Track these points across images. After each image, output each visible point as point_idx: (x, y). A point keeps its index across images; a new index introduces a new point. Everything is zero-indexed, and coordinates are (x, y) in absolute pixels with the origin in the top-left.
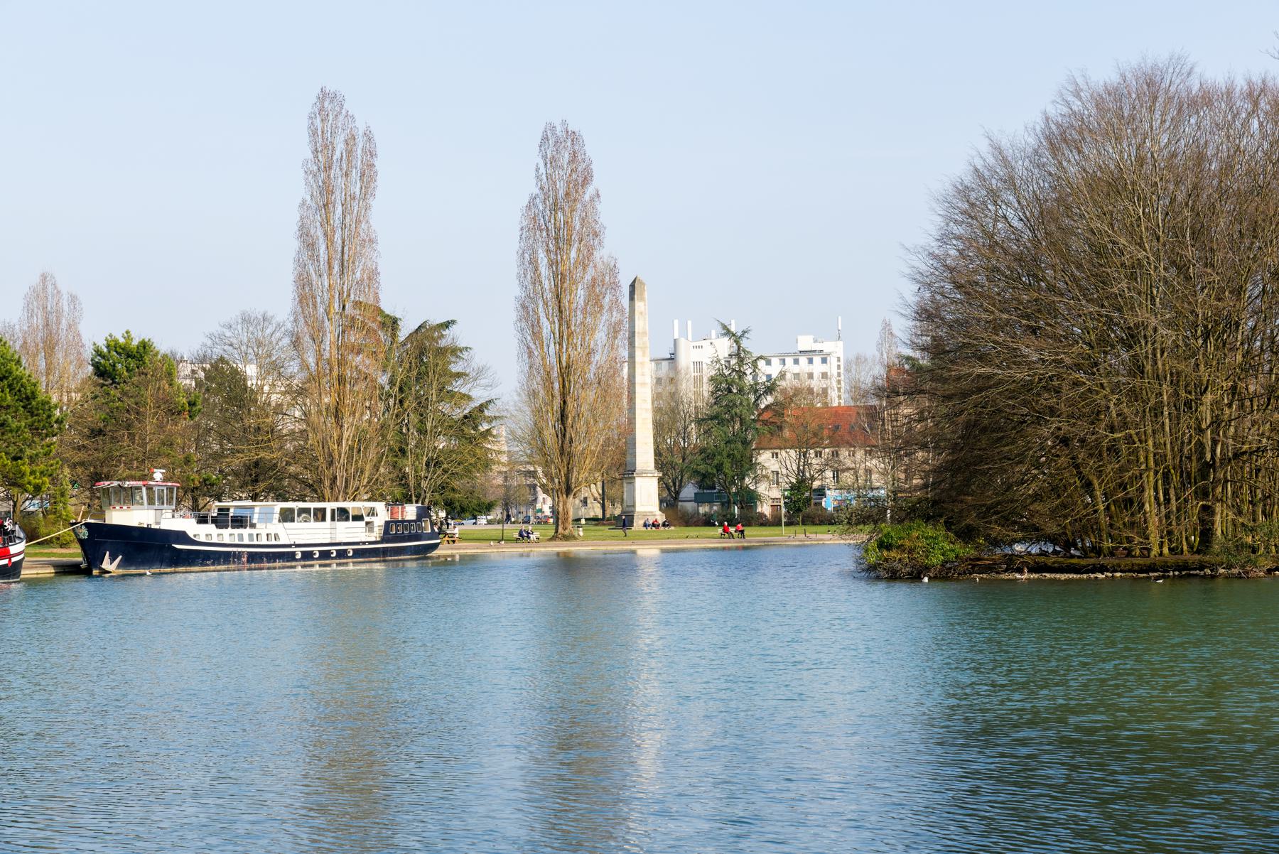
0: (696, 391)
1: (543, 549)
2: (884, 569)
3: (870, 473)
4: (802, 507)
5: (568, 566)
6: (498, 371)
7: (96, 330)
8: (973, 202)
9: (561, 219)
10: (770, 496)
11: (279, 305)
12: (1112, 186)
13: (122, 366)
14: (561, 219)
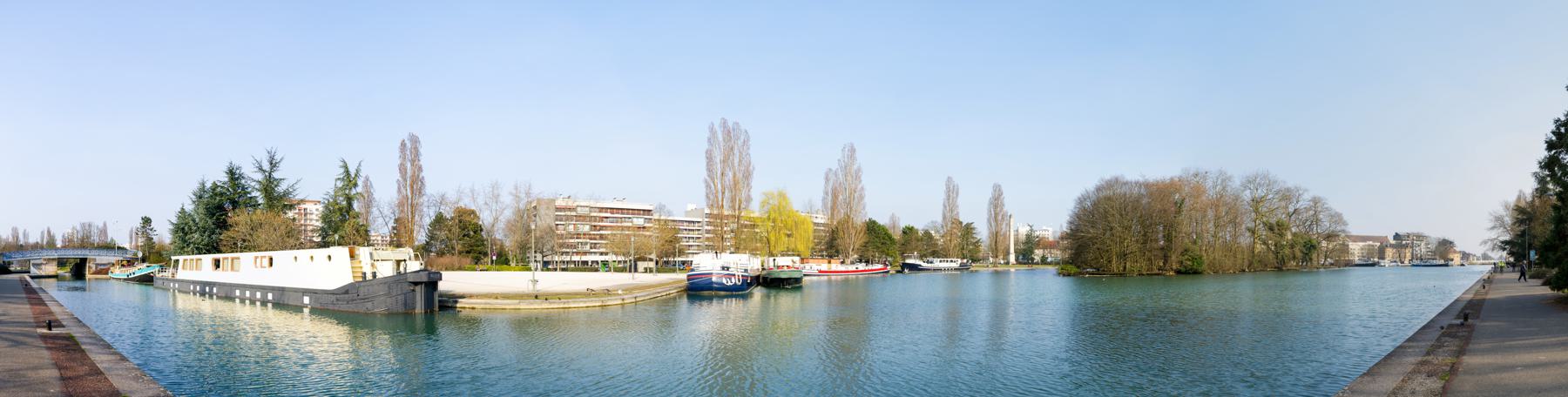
0: (1023, 237)
1: (992, 269)
2: (1064, 274)
3: (1057, 254)
4: (1044, 261)
5: (997, 272)
6: (983, 233)
7: (903, 224)
8: (1081, 201)
9: (996, 202)
10: (1037, 259)
11: (939, 219)
12: (1109, 199)
13: (908, 231)
14: (996, 202)
